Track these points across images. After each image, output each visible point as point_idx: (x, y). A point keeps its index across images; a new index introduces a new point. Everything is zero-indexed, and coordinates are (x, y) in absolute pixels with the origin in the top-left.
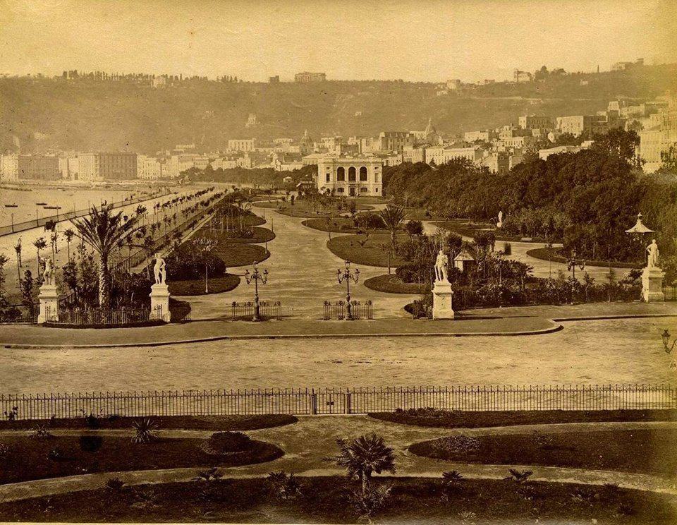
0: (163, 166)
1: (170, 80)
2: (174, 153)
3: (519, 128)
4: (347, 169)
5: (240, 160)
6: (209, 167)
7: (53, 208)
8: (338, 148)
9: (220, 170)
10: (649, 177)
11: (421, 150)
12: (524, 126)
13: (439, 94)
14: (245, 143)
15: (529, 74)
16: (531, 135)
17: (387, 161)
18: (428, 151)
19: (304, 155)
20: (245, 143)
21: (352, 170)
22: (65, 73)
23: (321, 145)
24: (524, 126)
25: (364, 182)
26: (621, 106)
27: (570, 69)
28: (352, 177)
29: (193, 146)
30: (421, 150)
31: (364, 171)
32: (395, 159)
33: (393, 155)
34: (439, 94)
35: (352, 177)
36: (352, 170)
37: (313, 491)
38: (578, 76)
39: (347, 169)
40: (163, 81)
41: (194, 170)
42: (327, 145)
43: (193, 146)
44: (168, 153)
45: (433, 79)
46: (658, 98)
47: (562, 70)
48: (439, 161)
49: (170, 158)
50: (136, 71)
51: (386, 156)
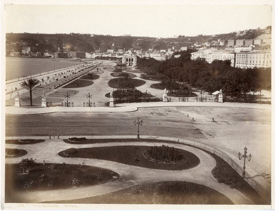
0: (92, 56)
1: (95, 35)
2: (94, 53)
3: (172, 49)
4: (128, 59)
5: (109, 55)
6: (102, 56)
7: (225, 107)
8: (131, 53)
9: (104, 57)
10: (166, 60)
11: (149, 54)
12: (173, 49)
13: (156, 40)
14: (239, 55)
15: (177, 36)
16: (175, 51)
17: (142, 56)
18: (150, 54)
19: (123, 54)
20: (239, 55)
21: (130, 59)
22: (71, 33)
23: (128, 52)
24: (173, 49)
25: (132, 62)
26: (197, 45)
27: (186, 36)
28: (130, 61)
29: (99, 51)
30: (149, 54)
31: (132, 60)
32: (143, 56)
33: (143, 55)
34: (156, 40)
35: (130, 61)
36: (130, 59)
37: (111, 201)
38: (188, 37)
39: (128, 59)
40: (93, 36)
41: (98, 57)
42: (129, 52)
43: (99, 51)
44: (93, 53)
45: (156, 37)
46: (205, 43)
47: (184, 36)
48: (210, 60)
49: (93, 54)
50: (87, 33)
51: (141, 55)
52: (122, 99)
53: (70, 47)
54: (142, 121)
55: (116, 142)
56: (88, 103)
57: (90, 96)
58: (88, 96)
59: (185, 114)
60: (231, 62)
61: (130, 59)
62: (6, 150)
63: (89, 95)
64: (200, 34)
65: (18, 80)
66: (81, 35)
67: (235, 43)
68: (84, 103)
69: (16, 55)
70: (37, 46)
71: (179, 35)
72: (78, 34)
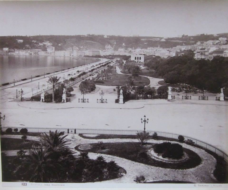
22: (87, 35)
52: (173, 163)
53: (26, 46)
54: (148, 119)
55: (124, 138)
56: (100, 100)
57: (103, 93)
58: (101, 93)
59: (155, 88)
60: (106, 47)
61: (138, 58)
62: (4, 181)
63: (102, 93)
64: (202, 33)
65: (44, 77)
66: (96, 36)
67: (72, 48)
68: (97, 99)
69: (77, 50)
70: (60, 46)
71: (183, 35)
72: (94, 35)
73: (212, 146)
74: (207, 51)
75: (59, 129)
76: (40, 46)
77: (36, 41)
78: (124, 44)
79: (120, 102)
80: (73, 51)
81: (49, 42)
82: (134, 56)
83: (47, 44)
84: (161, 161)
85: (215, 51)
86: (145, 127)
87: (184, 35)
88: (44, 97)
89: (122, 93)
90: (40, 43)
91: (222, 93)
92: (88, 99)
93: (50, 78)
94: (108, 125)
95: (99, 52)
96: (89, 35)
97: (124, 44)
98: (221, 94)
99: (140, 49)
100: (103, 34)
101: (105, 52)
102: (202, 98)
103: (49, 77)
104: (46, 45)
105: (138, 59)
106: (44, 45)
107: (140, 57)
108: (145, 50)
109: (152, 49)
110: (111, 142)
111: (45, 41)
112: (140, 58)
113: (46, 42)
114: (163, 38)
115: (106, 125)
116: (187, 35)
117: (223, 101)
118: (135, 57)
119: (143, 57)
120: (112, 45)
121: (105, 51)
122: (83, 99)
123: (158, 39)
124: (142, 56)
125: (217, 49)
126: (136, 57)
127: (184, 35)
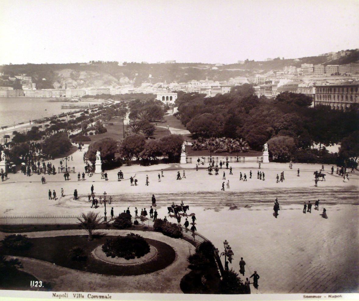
22: (90, 62)
61: (167, 98)
73: (200, 236)
74: (275, 84)
75: (64, 218)
76: (11, 82)
77: (4, 74)
78: (150, 76)
79: (96, 171)
80: (66, 88)
81: (26, 76)
82: (161, 95)
83: (22, 79)
84: (103, 262)
85: (286, 85)
86: (105, 211)
87: (247, 59)
88: (6, 166)
89: (99, 157)
90: (10, 77)
91: (266, 151)
92: (74, 168)
93: (133, 129)
94: (260, 210)
95: (109, 89)
96: (93, 62)
97: (150, 76)
98: (264, 152)
99: (176, 84)
100: (116, 61)
101: (120, 90)
102: (209, 160)
103: (279, 121)
104: (20, 80)
105: (168, 100)
106: (18, 80)
107: (171, 96)
108: (184, 86)
109: (195, 82)
110: (37, 237)
111: (20, 74)
112: (171, 98)
113: (20, 75)
114: (215, 64)
115: (337, 211)
116: (252, 60)
117: (268, 163)
118: (162, 96)
119: (175, 96)
120: (131, 77)
121: (120, 88)
122: (66, 167)
123: (208, 67)
124: (174, 95)
125: (289, 82)
126: (164, 96)
127: (247, 59)
